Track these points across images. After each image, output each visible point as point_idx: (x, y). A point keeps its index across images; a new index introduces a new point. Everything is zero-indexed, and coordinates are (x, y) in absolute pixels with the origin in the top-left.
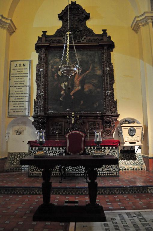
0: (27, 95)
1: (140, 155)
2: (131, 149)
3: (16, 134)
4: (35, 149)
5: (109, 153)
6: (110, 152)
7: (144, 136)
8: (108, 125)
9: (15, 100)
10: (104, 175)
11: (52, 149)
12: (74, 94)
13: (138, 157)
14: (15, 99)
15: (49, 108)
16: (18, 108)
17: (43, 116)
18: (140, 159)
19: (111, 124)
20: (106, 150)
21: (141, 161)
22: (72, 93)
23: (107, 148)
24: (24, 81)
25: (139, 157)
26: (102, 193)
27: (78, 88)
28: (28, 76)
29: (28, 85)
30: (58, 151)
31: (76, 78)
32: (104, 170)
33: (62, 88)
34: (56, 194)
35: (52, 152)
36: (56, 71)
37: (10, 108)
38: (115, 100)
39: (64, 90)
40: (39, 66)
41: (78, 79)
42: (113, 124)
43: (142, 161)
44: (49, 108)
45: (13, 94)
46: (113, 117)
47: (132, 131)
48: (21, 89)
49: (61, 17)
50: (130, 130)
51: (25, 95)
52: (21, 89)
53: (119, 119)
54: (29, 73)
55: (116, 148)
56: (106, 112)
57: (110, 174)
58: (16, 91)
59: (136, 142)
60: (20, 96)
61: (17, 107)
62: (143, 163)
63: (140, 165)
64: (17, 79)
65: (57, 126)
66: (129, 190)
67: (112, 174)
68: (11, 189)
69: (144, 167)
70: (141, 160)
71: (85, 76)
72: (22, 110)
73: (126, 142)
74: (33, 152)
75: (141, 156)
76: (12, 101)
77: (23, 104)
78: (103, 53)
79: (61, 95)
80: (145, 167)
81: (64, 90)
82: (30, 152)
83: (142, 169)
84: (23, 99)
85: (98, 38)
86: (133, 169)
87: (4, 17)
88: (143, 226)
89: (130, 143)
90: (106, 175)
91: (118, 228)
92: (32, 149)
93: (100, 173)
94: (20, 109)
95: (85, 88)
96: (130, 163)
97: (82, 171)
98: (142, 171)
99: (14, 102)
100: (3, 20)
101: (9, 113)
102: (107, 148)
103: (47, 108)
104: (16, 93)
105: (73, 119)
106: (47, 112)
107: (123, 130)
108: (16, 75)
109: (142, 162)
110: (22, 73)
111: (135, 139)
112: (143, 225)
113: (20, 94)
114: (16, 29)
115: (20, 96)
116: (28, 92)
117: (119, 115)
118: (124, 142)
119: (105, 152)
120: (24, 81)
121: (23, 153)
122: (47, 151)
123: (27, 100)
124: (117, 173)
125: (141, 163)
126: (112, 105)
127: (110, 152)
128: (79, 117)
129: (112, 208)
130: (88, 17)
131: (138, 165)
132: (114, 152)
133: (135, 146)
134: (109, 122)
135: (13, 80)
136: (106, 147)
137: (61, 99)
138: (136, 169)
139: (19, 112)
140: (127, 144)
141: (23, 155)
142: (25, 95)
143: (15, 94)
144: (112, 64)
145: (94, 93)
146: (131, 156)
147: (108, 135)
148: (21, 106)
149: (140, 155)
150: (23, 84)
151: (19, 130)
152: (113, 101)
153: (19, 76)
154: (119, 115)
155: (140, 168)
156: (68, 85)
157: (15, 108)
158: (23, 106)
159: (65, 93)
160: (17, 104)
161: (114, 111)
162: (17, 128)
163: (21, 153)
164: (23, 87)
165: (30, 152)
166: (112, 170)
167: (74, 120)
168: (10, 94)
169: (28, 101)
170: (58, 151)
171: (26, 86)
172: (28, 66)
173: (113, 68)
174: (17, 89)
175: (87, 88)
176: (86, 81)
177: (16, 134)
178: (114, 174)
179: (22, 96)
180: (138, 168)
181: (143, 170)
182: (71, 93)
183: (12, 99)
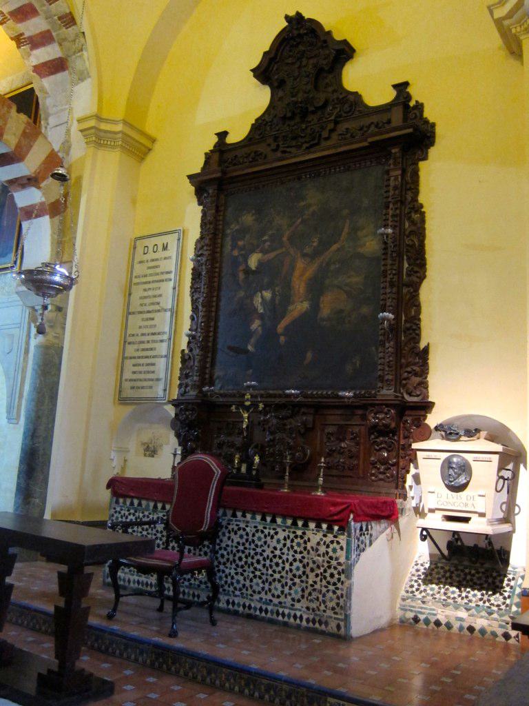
0: (165, 337)
3: (145, 455)
5: (318, 544)
6: (322, 543)
10: (298, 621)
12: (287, 328)
14: (138, 350)
15: (218, 377)
17: (193, 404)
20: (309, 534)
24: (160, 296)
27: (300, 307)
28: (171, 280)
29: (170, 307)
31: (297, 273)
32: (298, 605)
33: (256, 310)
36: (242, 255)
37: (124, 378)
38: (422, 345)
39: (261, 317)
40: (199, 245)
41: (301, 275)
44: (215, 377)
48: (153, 319)
49: (263, 73)
50: (447, 464)
51: (160, 337)
52: (153, 319)
54: (173, 269)
55: (342, 529)
57: (317, 625)
58: (140, 327)
59: (474, 518)
60: (148, 342)
61: (140, 372)
64: (145, 290)
65: (230, 434)
66: (263, 687)
67: (323, 627)
71: (324, 265)
72: (150, 383)
73: (432, 511)
77: (153, 364)
78: (387, 172)
81: (261, 317)
85: (375, 119)
86: (471, 629)
87: (103, 119)
90: (304, 623)
92: (117, 502)
93: (287, 611)
95: (322, 306)
96: (466, 601)
97: (233, 592)
99: (134, 358)
100: (103, 126)
101: (120, 391)
102: (312, 525)
103: (211, 377)
105: (246, 415)
108: (144, 280)
110: (158, 270)
111: (466, 505)
114: (154, 141)
116: (167, 330)
119: (306, 538)
120: (160, 296)
123: (164, 353)
124: (342, 624)
126: (407, 366)
127: (322, 543)
128: (264, 408)
130: (345, 52)
131: (495, 616)
132: (335, 544)
135: (138, 293)
137: (250, 348)
138: (483, 631)
139: (143, 388)
142: (160, 337)
144: (422, 206)
146: (487, 573)
150: (158, 304)
151: (151, 443)
153: (150, 282)
156: (273, 298)
157: (135, 376)
159: (263, 326)
162: (146, 436)
164: (158, 314)
166: (324, 611)
167: (248, 418)
169: (166, 356)
171: (165, 310)
172: (172, 252)
173: (423, 221)
174: (143, 320)
175: (328, 305)
176: (327, 282)
178: (329, 628)
183: (130, 350)
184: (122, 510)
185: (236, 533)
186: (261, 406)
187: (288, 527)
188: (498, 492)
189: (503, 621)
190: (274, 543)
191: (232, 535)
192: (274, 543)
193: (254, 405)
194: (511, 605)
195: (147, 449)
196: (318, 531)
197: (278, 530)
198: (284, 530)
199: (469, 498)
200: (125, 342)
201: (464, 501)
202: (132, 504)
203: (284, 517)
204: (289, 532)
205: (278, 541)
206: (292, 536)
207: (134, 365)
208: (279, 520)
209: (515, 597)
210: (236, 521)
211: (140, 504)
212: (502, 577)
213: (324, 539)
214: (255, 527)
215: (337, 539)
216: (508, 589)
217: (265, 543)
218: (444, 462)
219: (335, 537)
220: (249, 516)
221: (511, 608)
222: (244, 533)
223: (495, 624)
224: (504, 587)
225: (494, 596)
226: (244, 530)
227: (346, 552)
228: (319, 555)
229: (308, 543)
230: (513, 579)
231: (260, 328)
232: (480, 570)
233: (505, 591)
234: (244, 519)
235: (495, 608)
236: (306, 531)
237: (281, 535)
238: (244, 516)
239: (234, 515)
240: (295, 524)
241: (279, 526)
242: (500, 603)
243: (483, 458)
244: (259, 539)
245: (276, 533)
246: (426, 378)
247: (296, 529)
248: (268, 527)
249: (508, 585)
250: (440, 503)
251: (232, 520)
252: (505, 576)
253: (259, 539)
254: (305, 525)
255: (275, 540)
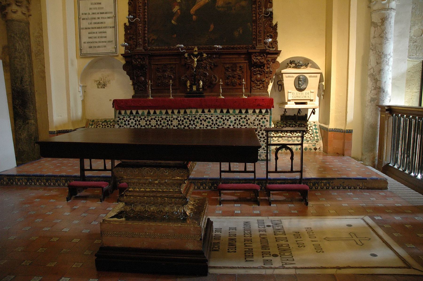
1: (315, 125)
2: (299, 115)
3: (98, 87)
4: (126, 113)
5: (254, 120)
7: (324, 91)
8: (259, 71)
9: (90, 26)
11: (155, 113)
12: (197, 11)
13: (311, 128)
14: (91, 23)
16: (97, 40)
18: (314, 131)
19: (265, 68)
20: (249, 116)
21: (315, 135)
22: (193, 10)
23: (252, 111)
25: (314, 127)
26: (198, 188)
30: (164, 117)
34: (200, 188)
35: (155, 119)
37: (82, 42)
38: (274, 23)
42: (268, 68)
43: (318, 134)
45: (86, 14)
46: (269, 56)
47: (300, 82)
53: (280, 59)
56: (257, 45)
58: (90, 9)
59: (308, 102)
60: (99, 18)
61: (95, 38)
62: (319, 138)
63: (312, 141)
68: (17, 179)
69: (320, 145)
70: (316, 133)
72: (105, 44)
73: (289, 101)
74: (123, 119)
75: (317, 127)
76: (84, 27)
77: (105, 32)
79: (174, 14)
80: (322, 145)
82: (118, 119)
83: (315, 149)
84: (105, 23)
88: (276, 241)
89: (296, 103)
91: (234, 242)
92: (120, 113)
94: (100, 42)
98: (315, 153)
99: (89, 28)
102: (250, 111)
104: (91, 12)
105: (196, 60)
106: (198, 47)
107: (285, 79)
109: (317, 136)
111: (305, 97)
112: (277, 240)
113: (98, 13)
115: (99, 18)
117: (281, 51)
118: (286, 101)
121: (112, 120)
122: (146, 117)
125: (316, 138)
129: (239, 212)
131: (310, 142)
132: (263, 119)
133: (308, 109)
134: (262, 65)
136: (249, 111)
137: (173, 22)
139: (99, 47)
140: (291, 105)
141: (112, 124)
143: (89, 14)
145: (235, 9)
147: (258, 89)
148: (102, 37)
149: (315, 125)
152: (271, 25)
154: (281, 51)
155: (313, 148)
157: (91, 40)
158: (105, 37)
160: (94, 33)
161: (271, 44)
163: (108, 121)
165: (118, 119)
167: (197, 61)
168: (81, 14)
170: (164, 117)
177: (98, 87)
179: (102, 18)
180: (308, 148)
181: (317, 151)
182: (191, 10)
184: (124, 117)
185: (205, 121)
186: (205, 55)
187: (236, 114)
188: (280, 91)
189: (314, 143)
190: (229, 123)
191: (203, 122)
192: (229, 123)
193: (201, 54)
194: (314, 137)
195: (99, 84)
196: (254, 114)
197: (231, 116)
198: (234, 116)
199: (306, 94)
200: (79, 18)
201: (304, 95)
202: (131, 113)
203: (234, 109)
204: (238, 116)
205: (231, 122)
206: (239, 118)
207: (89, 33)
208: (231, 111)
209: (315, 133)
210: (204, 115)
211: (137, 113)
212: (306, 127)
213: (257, 118)
214: (217, 116)
215: (264, 117)
216: (310, 131)
217: (224, 123)
218: (296, 78)
219: (263, 116)
220: (212, 111)
221: (314, 138)
222: (210, 120)
223: (311, 145)
224: (309, 130)
225: (306, 134)
226: (210, 118)
227: (270, 122)
228: (255, 126)
229: (248, 121)
230: (311, 126)
231: (179, 11)
232: (296, 125)
233: (310, 132)
234: (210, 113)
235: (309, 139)
236: (247, 115)
237: (233, 119)
238: (209, 111)
239: (203, 112)
240: (240, 112)
241: (231, 114)
242: (309, 137)
243: (311, 76)
244: (220, 122)
245: (230, 118)
246: (276, 39)
247: (241, 114)
248: (224, 116)
249: (310, 129)
250: (293, 97)
251: (202, 115)
252: (307, 126)
253: (220, 122)
254: (247, 112)
255: (229, 121)
